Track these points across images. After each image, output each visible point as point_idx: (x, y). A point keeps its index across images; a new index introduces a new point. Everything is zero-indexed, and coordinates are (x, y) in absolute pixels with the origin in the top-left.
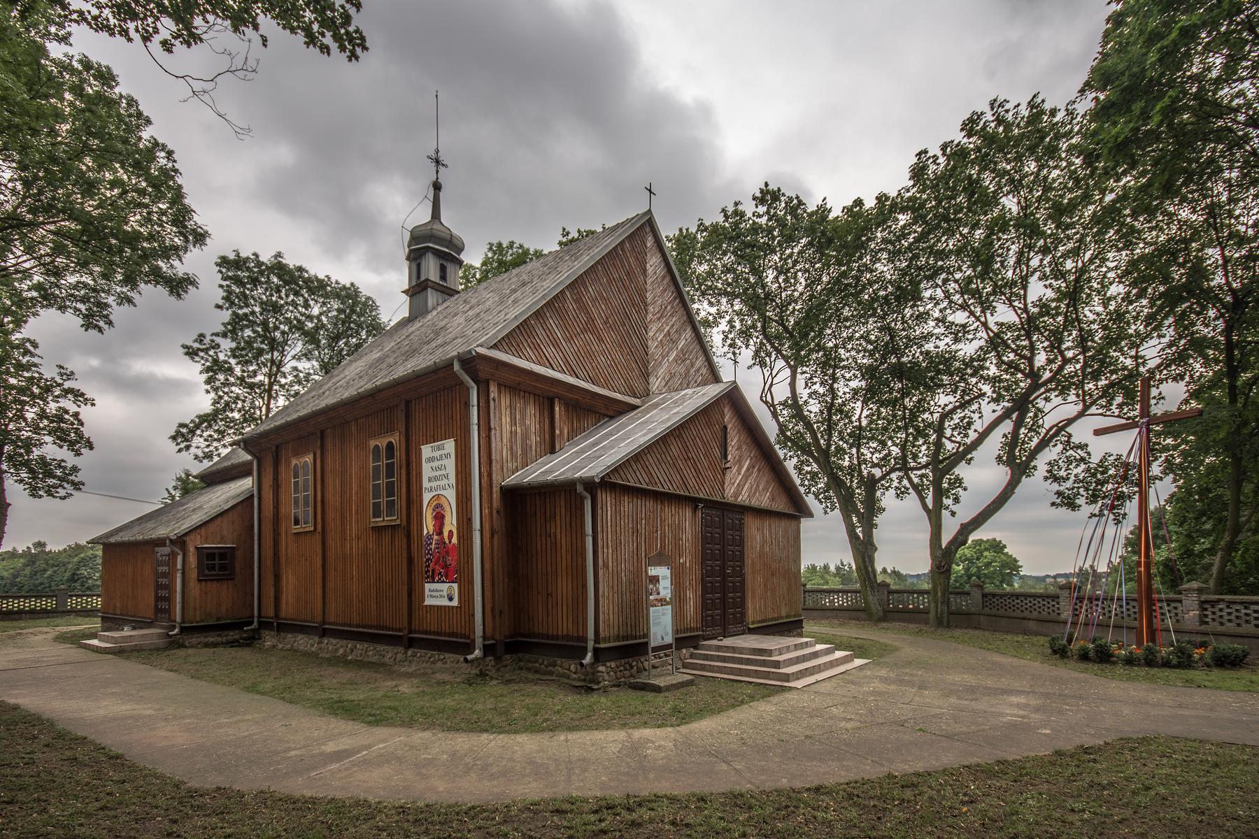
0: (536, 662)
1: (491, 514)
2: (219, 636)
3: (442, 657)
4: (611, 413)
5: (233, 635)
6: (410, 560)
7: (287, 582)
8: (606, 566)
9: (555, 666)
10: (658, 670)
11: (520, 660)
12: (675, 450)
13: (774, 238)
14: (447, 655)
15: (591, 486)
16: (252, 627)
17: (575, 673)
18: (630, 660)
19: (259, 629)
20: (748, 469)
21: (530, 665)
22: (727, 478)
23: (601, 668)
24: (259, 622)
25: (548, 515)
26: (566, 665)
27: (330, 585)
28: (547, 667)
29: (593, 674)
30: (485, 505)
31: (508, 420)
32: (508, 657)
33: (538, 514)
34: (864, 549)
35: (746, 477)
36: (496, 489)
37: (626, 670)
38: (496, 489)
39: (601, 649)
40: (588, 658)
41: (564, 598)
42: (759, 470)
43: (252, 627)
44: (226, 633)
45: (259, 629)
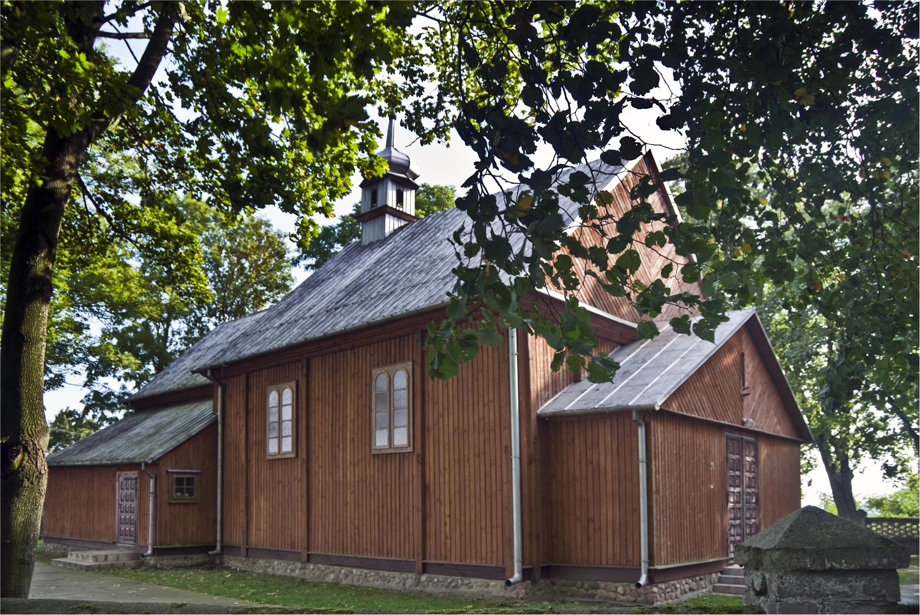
0: (574, 585)
1: (528, 441)
2: (186, 558)
3: (466, 581)
4: (623, 341)
5: (198, 558)
6: (425, 487)
7: (259, 508)
8: (658, 491)
9: (597, 588)
10: (696, 592)
11: (554, 584)
12: (707, 379)
13: (337, 85)
14: (473, 580)
15: (647, 414)
16: (216, 551)
17: (623, 595)
18: (675, 582)
19: (221, 554)
20: (760, 396)
21: (566, 589)
22: (745, 403)
23: (655, 589)
24: (222, 547)
25: (589, 441)
26: (612, 585)
27: (316, 510)
28: (587, 590)
29: (646, 594)
30: (524, 433)
31: (542, 351)
32: (542, 581)
33: (577, 442)
34: (391, 439)
35: (759, 403)
36: (533, 417)
37: (672, 591)
38: (533, 417)
39: (657, 570)
40: (643, 580)
41: (610, 525)
42: (769, 396)
43: (216, 551)
44: (190, 556)
45: (221, 554)
